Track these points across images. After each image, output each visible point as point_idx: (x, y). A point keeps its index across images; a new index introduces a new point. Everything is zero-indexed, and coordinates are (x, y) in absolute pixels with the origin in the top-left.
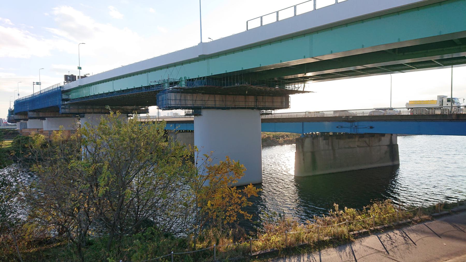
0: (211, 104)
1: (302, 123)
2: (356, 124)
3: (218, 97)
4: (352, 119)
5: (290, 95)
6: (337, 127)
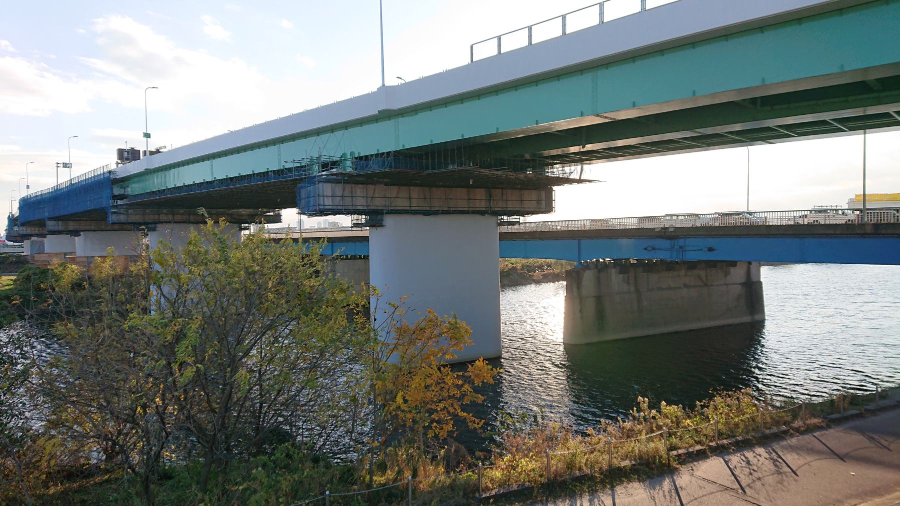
0: (402, 204)
1: (577, 241)
2: (681, 242)
3: (415, 192)
4: (673, 234)
5: (554, 188)
6: (646, 249)
